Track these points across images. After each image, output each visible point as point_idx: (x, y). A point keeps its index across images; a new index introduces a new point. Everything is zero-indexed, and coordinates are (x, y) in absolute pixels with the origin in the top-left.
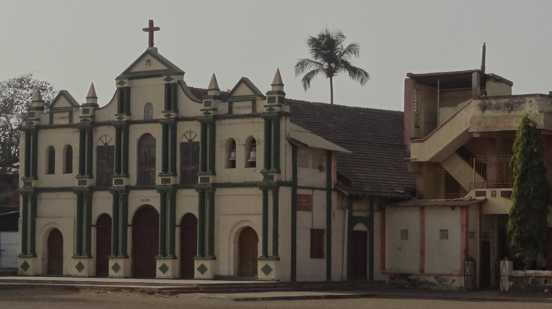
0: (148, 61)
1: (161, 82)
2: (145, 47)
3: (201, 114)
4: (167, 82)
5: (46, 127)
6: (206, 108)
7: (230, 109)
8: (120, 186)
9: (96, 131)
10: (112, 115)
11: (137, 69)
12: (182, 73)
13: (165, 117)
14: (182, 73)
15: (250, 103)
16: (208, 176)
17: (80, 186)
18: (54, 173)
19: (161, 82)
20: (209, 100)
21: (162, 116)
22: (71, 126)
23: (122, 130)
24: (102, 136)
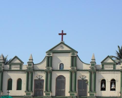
0: (62, 46)
1: (70, 55)
2: (60, 41)
3: (89, 69)
4: (72, 55)
5: (8, 71)
6: (92, 66)
7: (10, 68)
8: (48, 96)
9: (35, 73)
10: (44, 66)
11: (54, 49)
12: (77, 52)
13: (71, 69)
14: (77, 52)
15: (19, 66)
16: (30, 93)
17: (47, 96)
18: (12, 90)
19: (70, 55)
20: (94, 63)
21: (70, 69)
22: (21, 70)
23: (49, 73)
24: (84, 76)
